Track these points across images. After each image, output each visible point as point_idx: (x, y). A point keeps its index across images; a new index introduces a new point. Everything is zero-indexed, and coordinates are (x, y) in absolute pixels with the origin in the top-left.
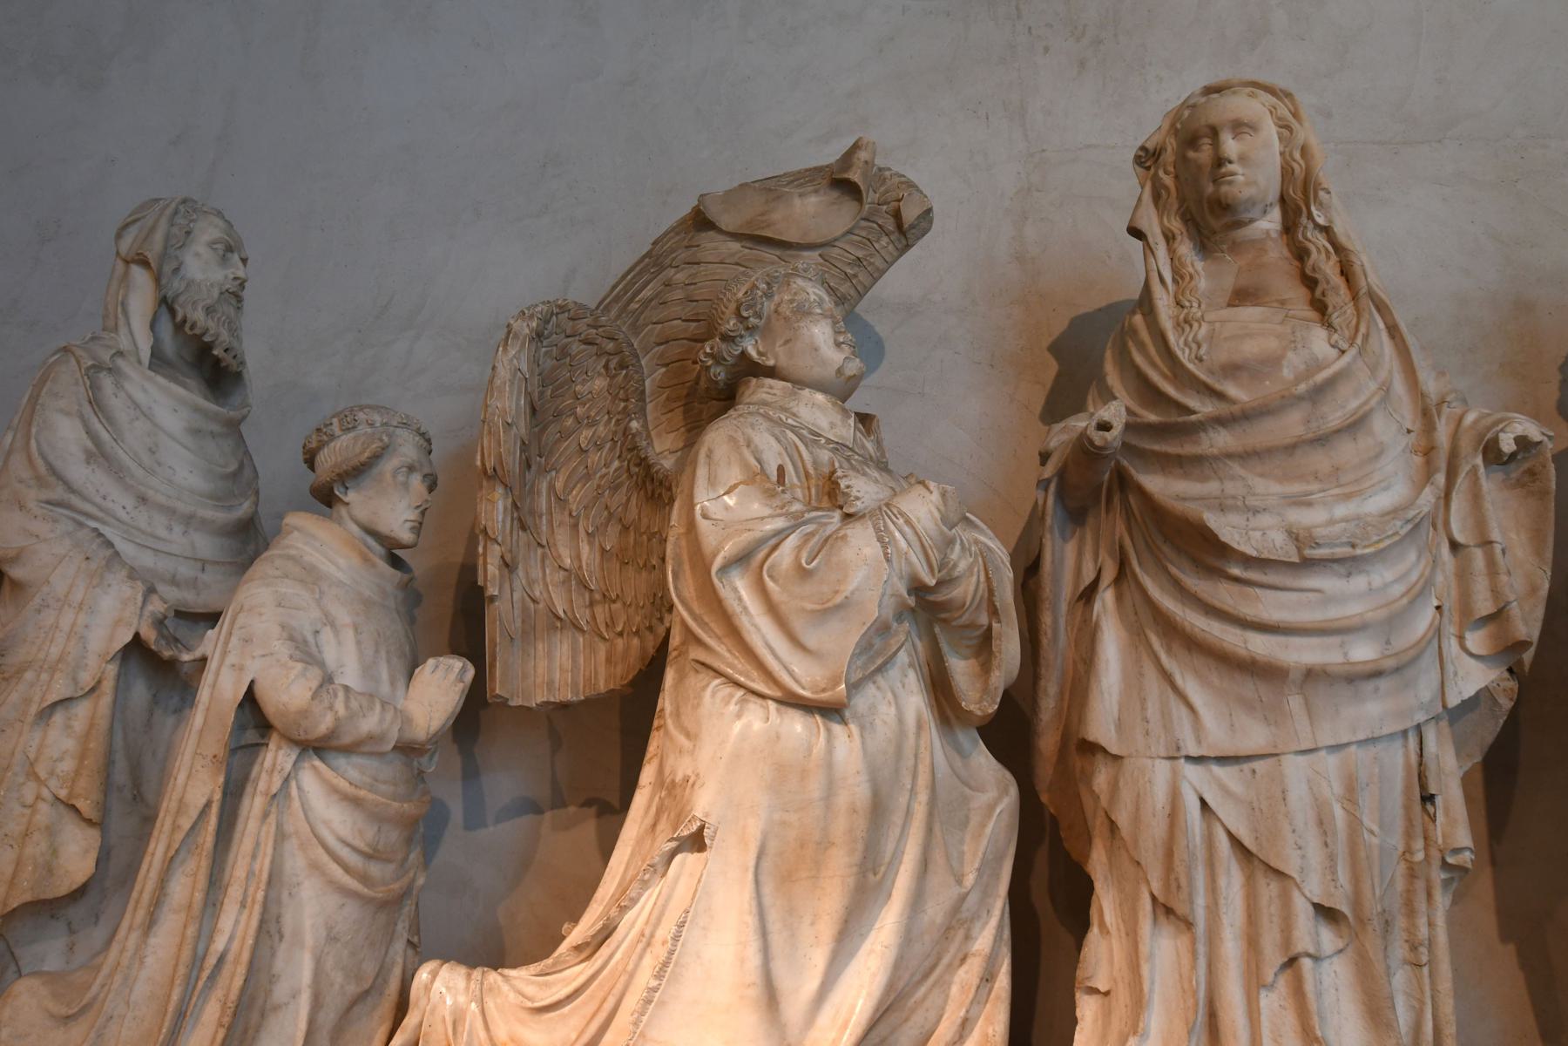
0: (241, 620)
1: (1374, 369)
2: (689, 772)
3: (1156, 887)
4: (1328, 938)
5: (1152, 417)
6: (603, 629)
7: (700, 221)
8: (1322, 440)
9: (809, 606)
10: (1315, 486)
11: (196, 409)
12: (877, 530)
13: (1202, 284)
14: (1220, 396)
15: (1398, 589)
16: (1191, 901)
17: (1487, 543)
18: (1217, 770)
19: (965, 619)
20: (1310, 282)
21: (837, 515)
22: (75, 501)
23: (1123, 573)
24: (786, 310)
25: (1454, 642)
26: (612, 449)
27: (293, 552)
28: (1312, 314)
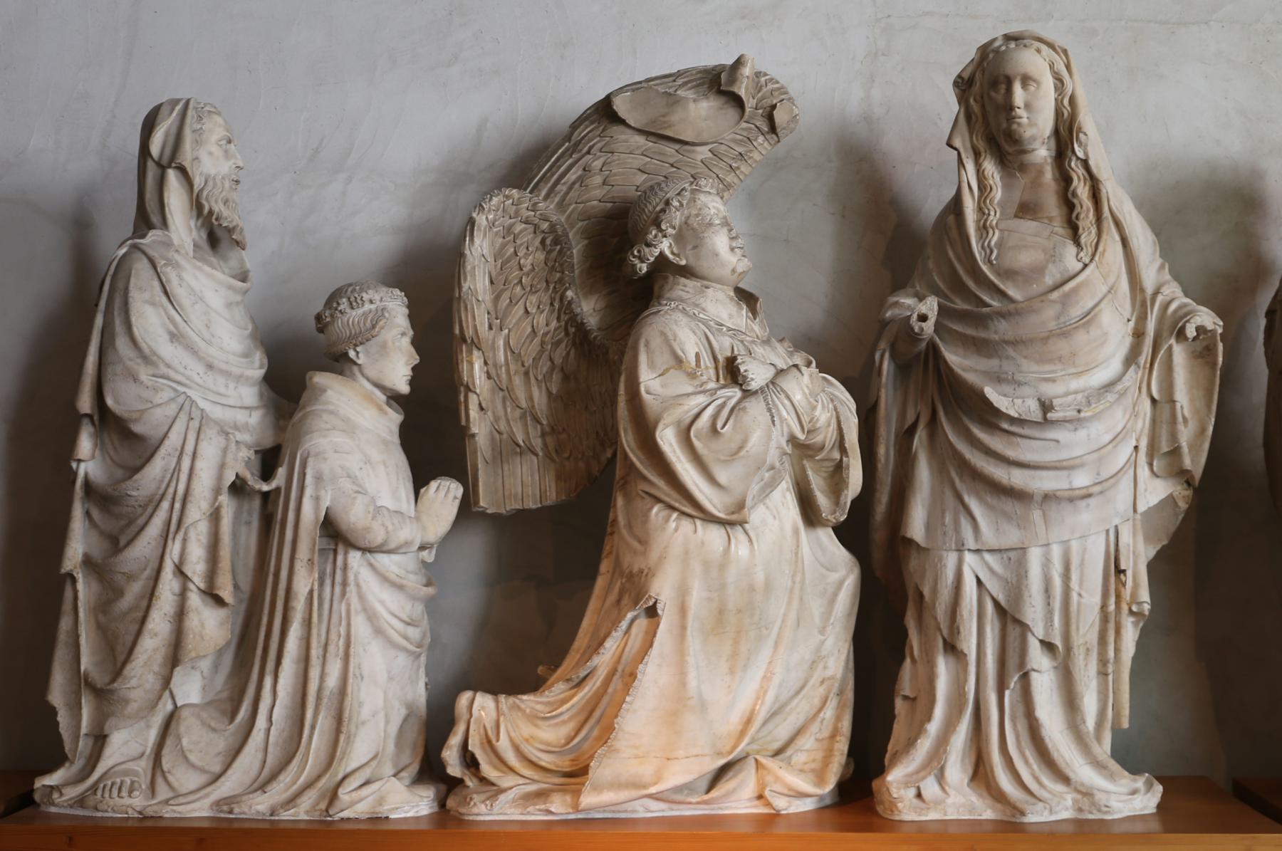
1: (1105, 277)
2: (643, 566)
3: (945, 632)
5: (961, 305)
6: (554, 455)
7: (605, 112)
9: (723, 458)
10: (1059, 367)
11: (230, 287)
12: (768, 404)
13: (998, 194)
14: (1003, 294)
18: (987, 556)
22: (172, 374)
24: (694, 222)
25: (1146, 468)
26: (552, 312)
27: (331, 407)
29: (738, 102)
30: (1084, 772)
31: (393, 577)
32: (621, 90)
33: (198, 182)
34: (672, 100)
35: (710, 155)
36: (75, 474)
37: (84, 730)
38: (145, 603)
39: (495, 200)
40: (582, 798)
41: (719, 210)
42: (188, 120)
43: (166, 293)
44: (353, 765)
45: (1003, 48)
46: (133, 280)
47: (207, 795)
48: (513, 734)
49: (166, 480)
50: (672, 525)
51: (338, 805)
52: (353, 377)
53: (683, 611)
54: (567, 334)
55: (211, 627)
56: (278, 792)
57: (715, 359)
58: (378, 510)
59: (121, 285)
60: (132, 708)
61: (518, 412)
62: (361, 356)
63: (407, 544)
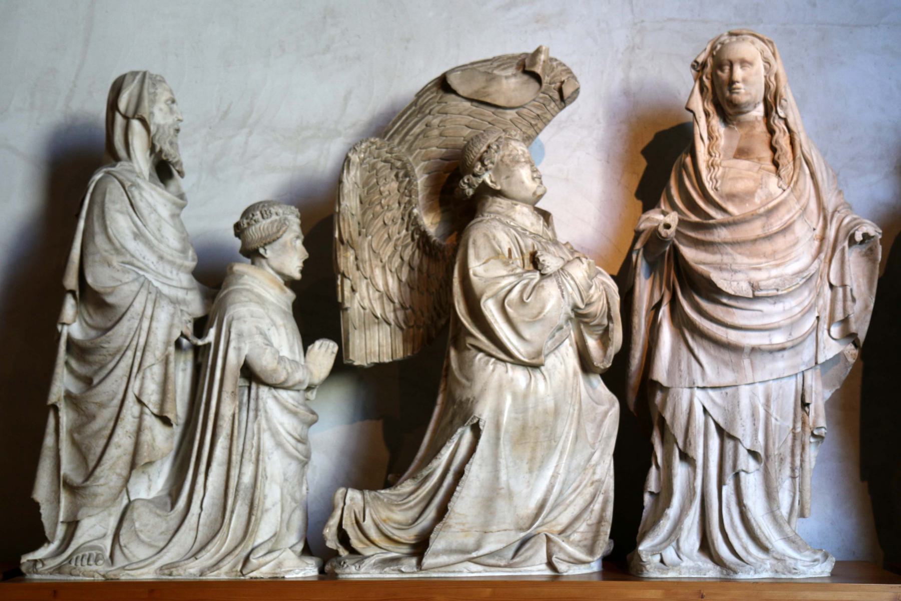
0: (234, 324)
1: (798, 199)
2: (469, 396)
4: (752, 464)
5: (694, 218)
6: (403, 325)
7: (443, 84)
8: (769, 237)
9: (527, 320)
10: (763, 260)
12: (559, 283)
13: (722, 142)
15: (798, 309)
16: (695, 450)
17: (844, 286)
18: (711, 392)
19: (595, 322)
20: (774, 150)
21: (538, 274)
22: (135, 262)
23: (674, 304)
24: (507, 160)
25: (826, 332)
26: (402, 224)
27: (248, 287)
28: (772, 168)
29: (537, 78)
30: (779, 544)
31: (290, 406)
32: (453, 70)
33: (153, 128)
34: (491, 78)
35: (517, 116)
36: (59, 335)
37: (61, 519)
38: (112, 424)
39: (363, 146)
40: (424, 560)
41: (524, 152)
42: (146, 85)
43: (132, 205)
44: (259, 541)
45: (728, 41)
46: (108, 196)
47: (153, 563)
48: (375, 516)
49: (131, 336)
50: (491, 367)
51: (250, 567)
52: (261, 266)
53: (497, 426)
54: (413, 239)
55: (162, 440)
56: (206, 558)
57: (522, 253)
58: (281, 359)
59: (98, 199)
60: (100, 500)
61: (377, 294)
62: (269, 253)
63: (300, 383)
